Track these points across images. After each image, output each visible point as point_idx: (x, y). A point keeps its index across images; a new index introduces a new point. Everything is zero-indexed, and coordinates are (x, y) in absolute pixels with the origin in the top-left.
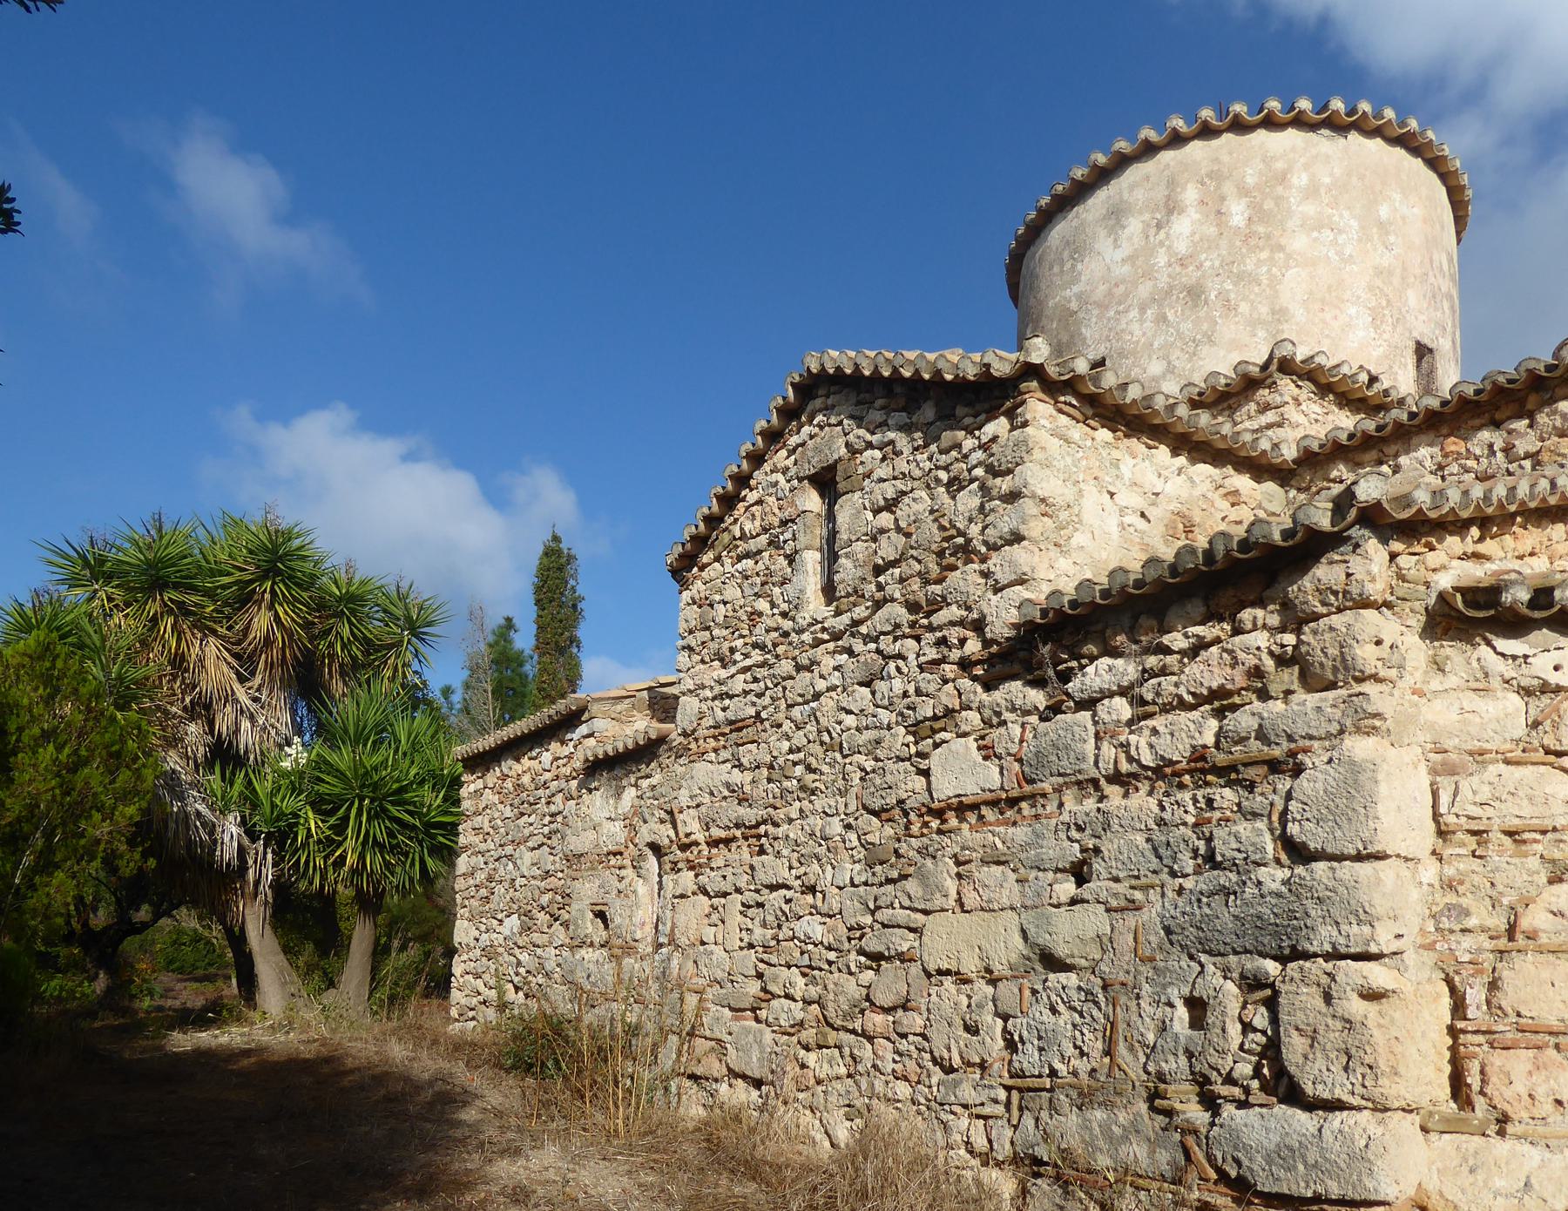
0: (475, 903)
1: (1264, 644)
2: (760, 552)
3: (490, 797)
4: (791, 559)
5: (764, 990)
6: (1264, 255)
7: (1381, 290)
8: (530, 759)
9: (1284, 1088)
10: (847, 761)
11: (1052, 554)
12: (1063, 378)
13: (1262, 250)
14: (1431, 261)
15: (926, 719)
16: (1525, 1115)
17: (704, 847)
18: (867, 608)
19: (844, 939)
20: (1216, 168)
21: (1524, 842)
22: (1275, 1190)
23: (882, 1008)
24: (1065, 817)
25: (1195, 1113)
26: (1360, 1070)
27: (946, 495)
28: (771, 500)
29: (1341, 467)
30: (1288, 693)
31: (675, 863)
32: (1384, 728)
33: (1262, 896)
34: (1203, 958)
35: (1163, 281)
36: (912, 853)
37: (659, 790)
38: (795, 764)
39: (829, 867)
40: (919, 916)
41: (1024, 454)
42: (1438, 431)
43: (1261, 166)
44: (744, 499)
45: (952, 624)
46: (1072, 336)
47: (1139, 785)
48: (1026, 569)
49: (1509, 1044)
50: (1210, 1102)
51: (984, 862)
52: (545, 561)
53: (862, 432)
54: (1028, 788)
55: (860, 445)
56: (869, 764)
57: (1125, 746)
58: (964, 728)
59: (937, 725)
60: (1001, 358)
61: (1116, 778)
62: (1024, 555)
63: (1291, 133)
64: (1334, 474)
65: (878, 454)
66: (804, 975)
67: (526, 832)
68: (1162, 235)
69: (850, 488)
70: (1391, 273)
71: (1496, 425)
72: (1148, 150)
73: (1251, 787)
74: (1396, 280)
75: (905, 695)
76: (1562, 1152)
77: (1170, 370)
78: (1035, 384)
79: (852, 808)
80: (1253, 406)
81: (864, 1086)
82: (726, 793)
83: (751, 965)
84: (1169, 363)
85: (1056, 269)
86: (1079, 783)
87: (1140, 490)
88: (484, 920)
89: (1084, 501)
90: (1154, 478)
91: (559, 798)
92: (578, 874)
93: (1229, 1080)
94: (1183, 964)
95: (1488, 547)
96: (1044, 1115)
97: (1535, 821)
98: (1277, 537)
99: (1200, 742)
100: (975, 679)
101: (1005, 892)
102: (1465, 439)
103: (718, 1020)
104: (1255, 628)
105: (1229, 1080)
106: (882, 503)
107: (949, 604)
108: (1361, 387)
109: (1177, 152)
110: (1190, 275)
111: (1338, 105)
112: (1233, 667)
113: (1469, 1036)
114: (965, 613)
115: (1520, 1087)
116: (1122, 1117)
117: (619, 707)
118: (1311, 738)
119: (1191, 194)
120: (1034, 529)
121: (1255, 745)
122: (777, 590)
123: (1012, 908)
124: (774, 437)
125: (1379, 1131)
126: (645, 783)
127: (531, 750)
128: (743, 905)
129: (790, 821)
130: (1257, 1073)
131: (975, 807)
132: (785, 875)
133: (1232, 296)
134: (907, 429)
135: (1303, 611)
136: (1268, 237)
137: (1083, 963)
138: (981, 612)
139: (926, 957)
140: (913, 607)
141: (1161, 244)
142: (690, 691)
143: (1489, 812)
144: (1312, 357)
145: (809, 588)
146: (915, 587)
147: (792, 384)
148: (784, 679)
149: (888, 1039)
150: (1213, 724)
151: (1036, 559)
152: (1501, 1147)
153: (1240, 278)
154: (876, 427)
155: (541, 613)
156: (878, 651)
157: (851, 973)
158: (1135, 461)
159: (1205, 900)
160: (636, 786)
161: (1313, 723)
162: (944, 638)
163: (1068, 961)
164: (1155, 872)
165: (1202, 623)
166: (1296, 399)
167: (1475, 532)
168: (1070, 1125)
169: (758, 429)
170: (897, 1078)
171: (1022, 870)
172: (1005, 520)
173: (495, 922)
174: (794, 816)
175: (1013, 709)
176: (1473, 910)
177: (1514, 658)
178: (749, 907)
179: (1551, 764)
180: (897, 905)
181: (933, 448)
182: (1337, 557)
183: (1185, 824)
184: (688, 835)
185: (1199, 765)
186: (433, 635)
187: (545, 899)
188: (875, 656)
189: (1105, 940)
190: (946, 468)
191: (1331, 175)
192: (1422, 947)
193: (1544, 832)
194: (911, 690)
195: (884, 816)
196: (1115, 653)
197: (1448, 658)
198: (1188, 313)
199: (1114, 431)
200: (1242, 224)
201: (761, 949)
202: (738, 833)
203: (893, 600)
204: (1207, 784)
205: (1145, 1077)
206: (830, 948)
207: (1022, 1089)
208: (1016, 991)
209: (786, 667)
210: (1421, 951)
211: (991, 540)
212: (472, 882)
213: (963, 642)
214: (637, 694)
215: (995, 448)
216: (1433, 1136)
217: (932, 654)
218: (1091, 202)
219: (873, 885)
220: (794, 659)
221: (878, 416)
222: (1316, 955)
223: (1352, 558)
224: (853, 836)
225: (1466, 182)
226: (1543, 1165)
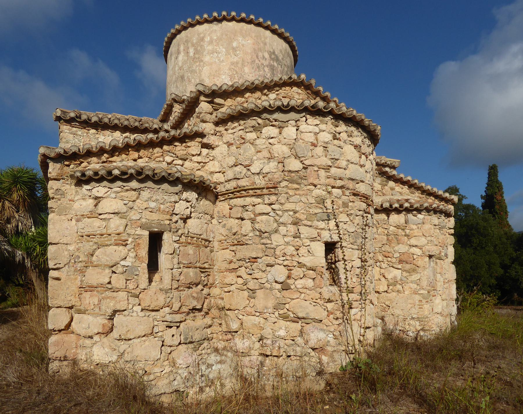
6: (198, 64)
43: (197, 36)
97: (92, 233)
115: (87, 302)
119: (182, 48)
133: (190, 77)
136: (199, 58)
191: (217, 36)
199: (97, 130)
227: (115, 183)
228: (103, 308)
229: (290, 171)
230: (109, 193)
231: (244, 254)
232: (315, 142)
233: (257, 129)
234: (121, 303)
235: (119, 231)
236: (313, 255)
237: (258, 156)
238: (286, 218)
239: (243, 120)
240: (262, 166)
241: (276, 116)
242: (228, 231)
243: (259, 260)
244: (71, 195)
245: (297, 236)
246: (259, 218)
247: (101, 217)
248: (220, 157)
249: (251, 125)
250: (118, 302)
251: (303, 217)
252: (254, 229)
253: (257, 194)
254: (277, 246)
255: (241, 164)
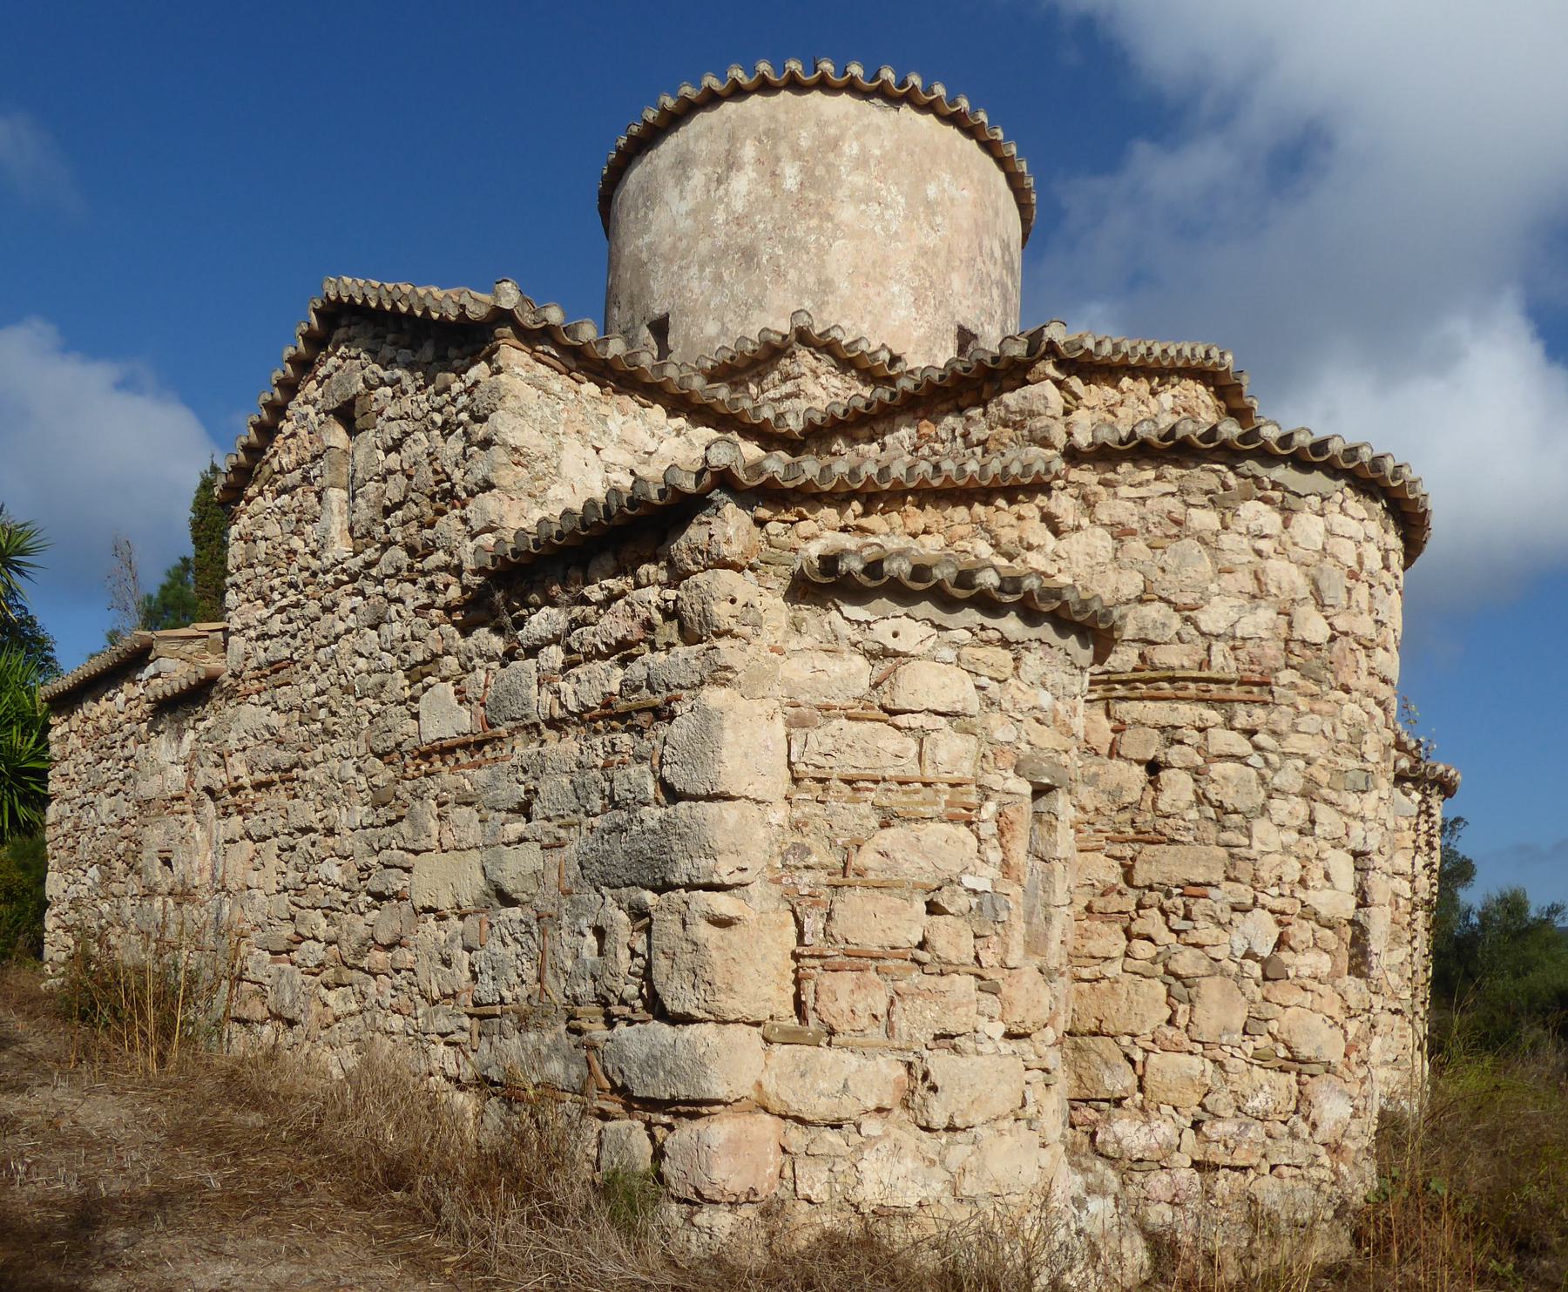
0: (63, 853)
1: (654, 599)
2: (295, 487)
3: (74, 741)
4: (319, 496)
5: (297, 933)
6: (814, 222)
7: (925, 271)
8: (107, 700)
9: (656, 1007)
10: (359, 704)
11: (525, 505)
12: (535, 327)
13: (811, 217)
14: (981, 247)
15: (418, 663)
16: (847, 1027)
17: (250, 790)
18: (376, 550)
19: (355, 879)
20: (773, 126)
21: (858, 790)
22: (645, 1094)
23: (382, 945)
24: (514, 761)
25: (598, 1031)
26: (702, 987)
27: (440, 438)
28: (303, 433)
29: (840, 441)
30: (669, 645)
31: (226, 807)
32: (736, 680)
33: (644, 833)
34: (604, 890)
35: (721, 239)
36: (406, 796)
37: (215, 733)
38: (320, 707)
39: (344, 810)
40: (411, 856)
41: (496, 401)
42: (915, 412)
44: (280, 431)
45: (439, 569)
46: (642, 289)
47: (569, 730)
48: (493, 517)
49: (837, 967)
50: (610, 1022)
51: (458, 804)
52: (203, 493)
53: (376, 367)
54: (490, 732)
55: (374, 381)
56: (375, 708)
57: (557, 692)
58: (445, 673)
59: (426, 669)
60: (476, 300)
61: (553, 723)
62: (493, 503)
63: (845, 98)
64: (835, 448)
65: (389, 391)
66: (326, 916)
67: (105, 777)
68: (721, 192)
69: (366, 425)
70: (936, 254)
71: (960, 410)
72: (712, 100)
73: (641, 733)
74: (940, 262)
75: (403, 640)
76: (875, 1058)
77: (724, 331)
78: (508, 330)
79: (362, 751)
80: (776, 375)
81: (369, 1021)
82: (268, 736)
83: (284, 908)
84: (723, 324)
85: (632, 216)
86: (526, 727)
87: (630, 448)
88: (71, 871)
89: (564, 454)
90: (647, 438)
91: (130, 742)
92: (147, 821)
93: (623, 1002)
94: (591, 896)
95: (874, 521)
96: (496, 1039)
97: (870, 772)
98: (654, 495)
99: (608, 690)
100: (454, 624)
101: (472, 832)
102: (936, 423)
103: (258, 963)
104: (649, 584)
105: (623, 1002)
106: (390, 443)
107: (438, 549)
108: (882, 365)
109: (739, 105)
110: (745, 237)
111: (888, 74)
112: (633, 617)
113: (807, 960)
114: (448, 558)
115: (844, 1004)
116: (549, 1037)
117: (189, 648)
118: (681, 687)
119: (749, 151)
120: (505, 477)
121: (645, 692)
122: (309, 528)
123: (477, 848)
124: (304, 366)
125: (717, 1040)
126: (201, 726)
127: (107, 691)
128: (279, 848)
129: (316, 764)
130: (641, 996)
131: (451, 750)
132: (313, 818)
133: (782, 262)
134: (410, 367)
135: (681, 568)
136: (818, 204)
137: (525, 897)
138: (460, 559)
139: (413, 896)
140: (411, 551)
141: (721, 200)
142: (239, 631)
143: (832, 762)
144: (828, 330)
145: (333, 527)
146: (413, 531)
147: (315, 310)
148: (313, 620)
149: (387, 975)
150: (619, 672)
151: (506, 507)
152: (827, 1055)
153: (790, 243)
154: (388, 363)
155: (199, 553)
156: (385, 595)
157: (362, 914)
158: (625, 418)
159: (606, 837)
160: (194, 728)
161: (682, 674)
162: (432, 582)
163: (514, 896)
164: (574, 812)
165: (613, 577)
166: (814, 371)
167: (856, 506)
168: (514, 1045)
169: (286, 357)
170: (394, 1012)
171: (484, 811)
172: (480, 467)
173: (81, 873)
174: (318, 759)
175: (481, 656)
176: (814, 849)
177: (859, 623)
178: (284, 850)
179: (885, 721)
180: (394, 846)
181: (431, 389)
182: (704, 519)
183: (596, 766)
184: (236, 779)
185: (607, 711)
186: (32, 566)
187: (121, 847)
188: (382, 599)
189: (539, 875)
190: (440, 410)
191: (882, 146)
192: (772, 881)
193: (876, 782)
194: (408, 635)
195: (387, 759)
196: (552, 603)
197: (804, 620)
198: (741, 275)
199: (602, 386)
200: (794, 189)
201: (292, 892)
202: (275, 776)
203: (396, 543)
204: (614, 730)
205: (565, 1001)
206: (344, 889)
207: (482, 1013)
208: (477, 925)
209: (313, 608)
210: (771, 884)
211: (469, 486)
212: (60, 831)
213: (447, 586)
214: (211, 635)
215: (476, 394)
216: (775, 1047)
217: (424, 598)
218: (663, 147)
219: (377, 827)
220: (320, 600)
221: (387, 352)
222: (678, 887)
223: (716, 521)
224: (362, 779)
225: (1025, 170)
226: (860, 1069)
227: (959, 614)
228: (902, 1024)
229: (1304, 642)
230: (930, 643)
231: (1166, 869)
232: (1356, 567)
233: (1217, 501)
234: (962, 1011)
235: (961, 775)
236: (1333, 888)
237: (1223, 585)
238: (1289, 778)
239: (1176, 467)
240: (1234, 616)
241: (1281, 473)
242: (1105, 797)
243: (1211, 891)
244: (777, 629)
245: (1307, 829)
246: (1217, 769)
247: (902, 720)
248: (1082, 564)
249: (1206, 487)
250: (952, 1007)
251: (1324, 777)
252: (1201, 799)
253: (1207, 695)
254: (1264, 853)
255: (1161, 598)
